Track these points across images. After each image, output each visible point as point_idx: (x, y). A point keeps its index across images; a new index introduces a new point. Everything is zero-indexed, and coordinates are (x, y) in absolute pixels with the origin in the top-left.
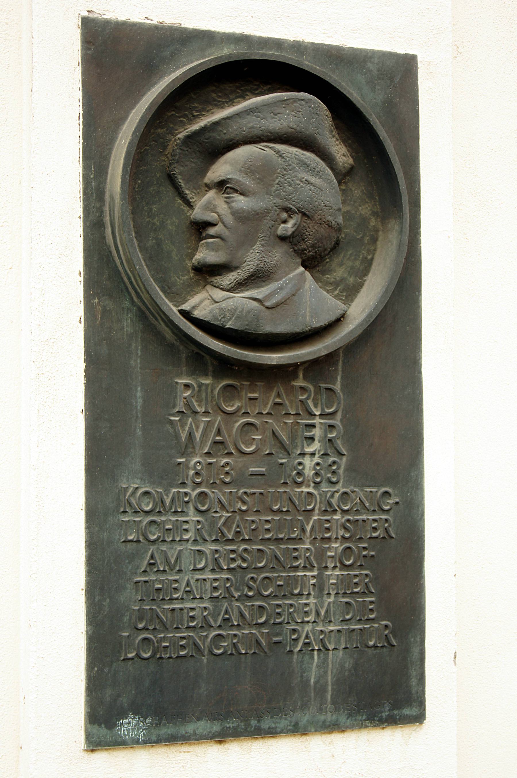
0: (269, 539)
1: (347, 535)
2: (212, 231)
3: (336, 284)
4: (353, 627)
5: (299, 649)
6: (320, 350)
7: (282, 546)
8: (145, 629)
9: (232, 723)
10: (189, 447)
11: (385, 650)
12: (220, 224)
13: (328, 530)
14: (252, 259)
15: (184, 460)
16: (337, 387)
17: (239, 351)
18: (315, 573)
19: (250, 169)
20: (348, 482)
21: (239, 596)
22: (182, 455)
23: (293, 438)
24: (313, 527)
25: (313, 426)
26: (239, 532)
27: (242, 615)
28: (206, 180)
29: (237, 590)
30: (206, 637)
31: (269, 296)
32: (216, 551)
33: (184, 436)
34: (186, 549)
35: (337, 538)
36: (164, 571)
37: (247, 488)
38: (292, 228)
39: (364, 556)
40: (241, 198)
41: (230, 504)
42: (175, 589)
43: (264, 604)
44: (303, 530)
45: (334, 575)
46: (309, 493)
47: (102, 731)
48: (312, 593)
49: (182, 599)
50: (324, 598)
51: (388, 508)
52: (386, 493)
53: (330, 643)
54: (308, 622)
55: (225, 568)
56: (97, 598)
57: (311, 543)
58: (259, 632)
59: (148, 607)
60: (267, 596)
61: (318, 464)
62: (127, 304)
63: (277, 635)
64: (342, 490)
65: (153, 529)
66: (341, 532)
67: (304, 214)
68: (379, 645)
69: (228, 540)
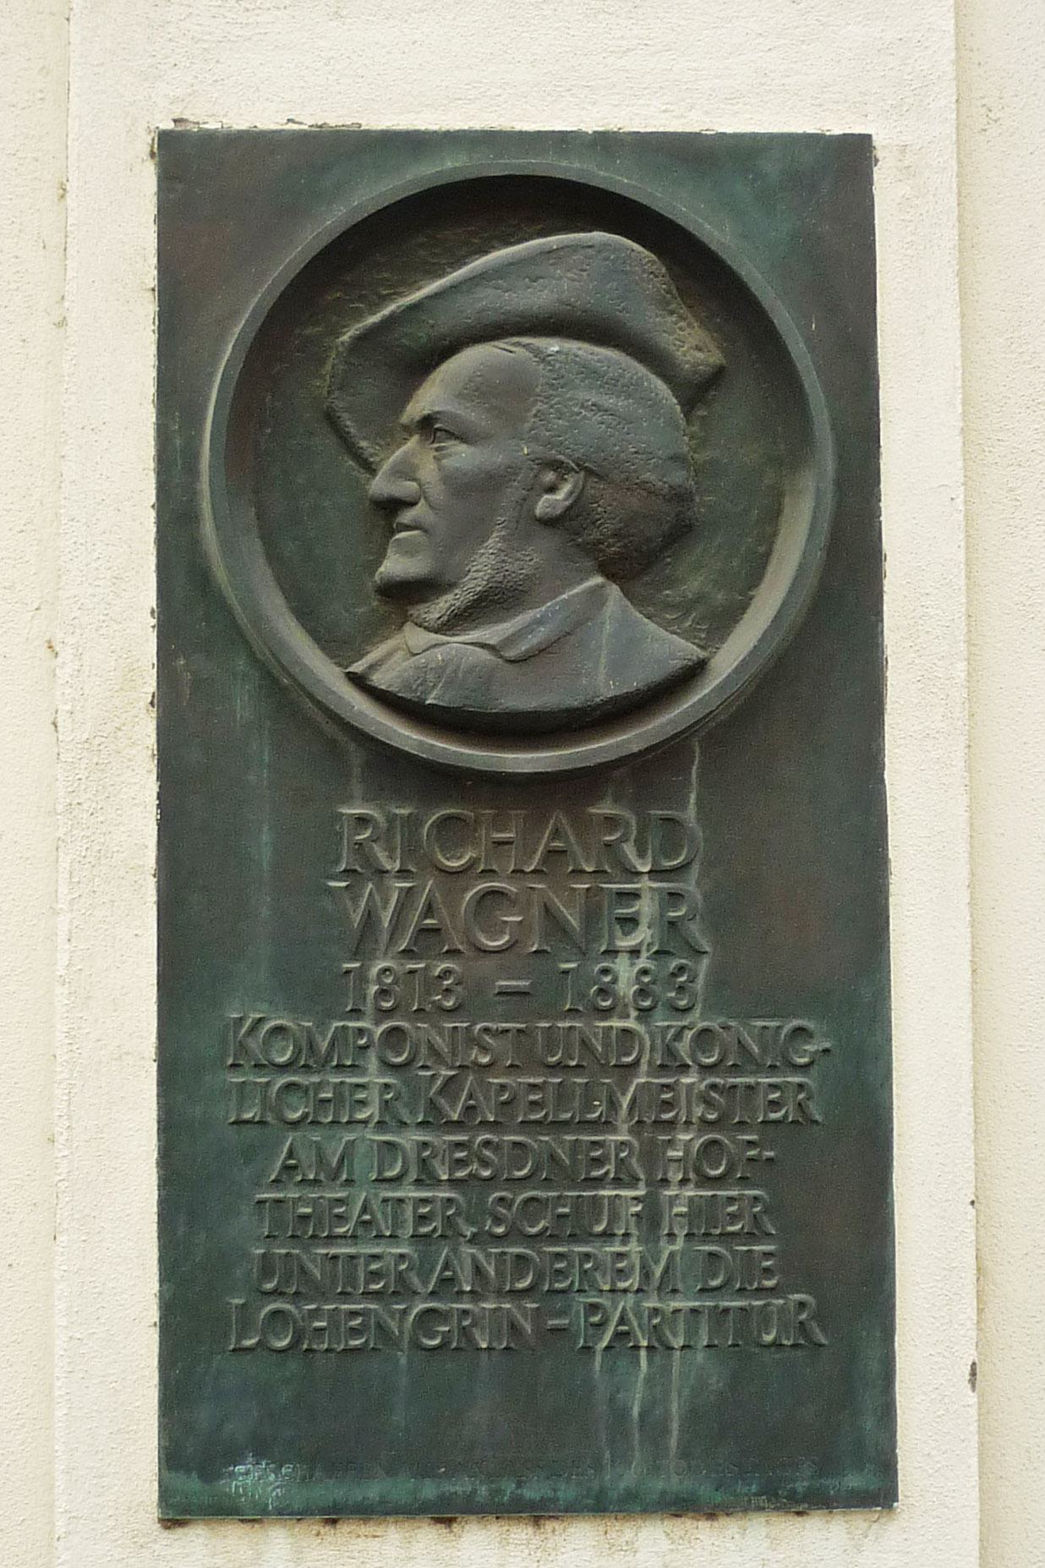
0: (538, 1122)
1: (712, 1117)
2: (407, 516)
3: (686, 607)
4: (727, 1304)
5: (605, 1344)
6: (628, 741)
7: (568, 1138)
8: (277, 1293)
9: (460, 1486)
10: (364, 941)
11: (799, 1353)
12: (422, 501)
13: (668, 1105)
14: (481, 569)
15: (357, 965)
16: (690, 814)
17: (453, 748)
18: (641, 1192)
19: (480, 390)
20: (709, 1010)
21: (474, 1235)
22: (355, 955)
23: (591, 917)
24: (634, 1101)
25: (635, 895)
26: (473, 1107)
27: (478, 1270)
28: (405, 419)
29: (471, 1221)
30: (405, 1312)
31: (509, 641)
32: (425, 1145)
33: (357, 918)
34: (363, 1139)
35: (688, 1123)
36: (316, 1181)
37: (493, 1021)
38: (565, 499)
39: (751, 1160)
40: (462, 449)
41: (454, 1054)
42: (339, 1217)
43: (528, 1251)
44: (613, 1105)
45: (681, 1197)
46: (625, 1031)
47: (192, 1484)
48: (634, 1231)
49: (354, 1237)
50: (662, 1244)
51: (802, 1061)
52: (800, 1030)
53: (675, 1335)
54: (625, 1291)
55: (445, 1177)
56: (181, 1231)
57: (630, 1131)
58: (519, 1307)
59: (283, 1251)
60: (536, 1236)
61: (645, 972)
62: (241, 664)
63: (561, 1314)
64: (702, 1025)
65: (293, 1099)
66: (698, 1111)
67: (590, 472)
68: (785, 1342)
69: (450, 1123)
